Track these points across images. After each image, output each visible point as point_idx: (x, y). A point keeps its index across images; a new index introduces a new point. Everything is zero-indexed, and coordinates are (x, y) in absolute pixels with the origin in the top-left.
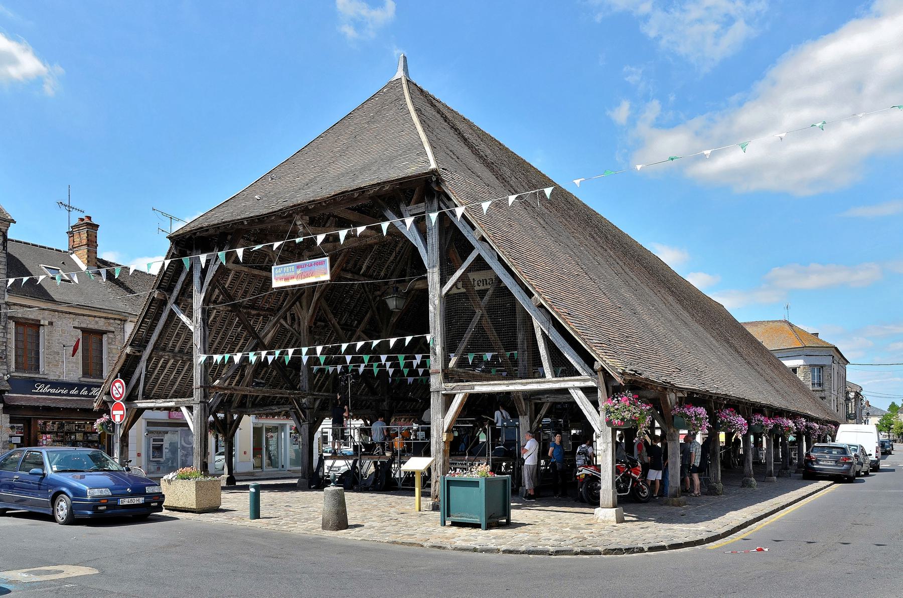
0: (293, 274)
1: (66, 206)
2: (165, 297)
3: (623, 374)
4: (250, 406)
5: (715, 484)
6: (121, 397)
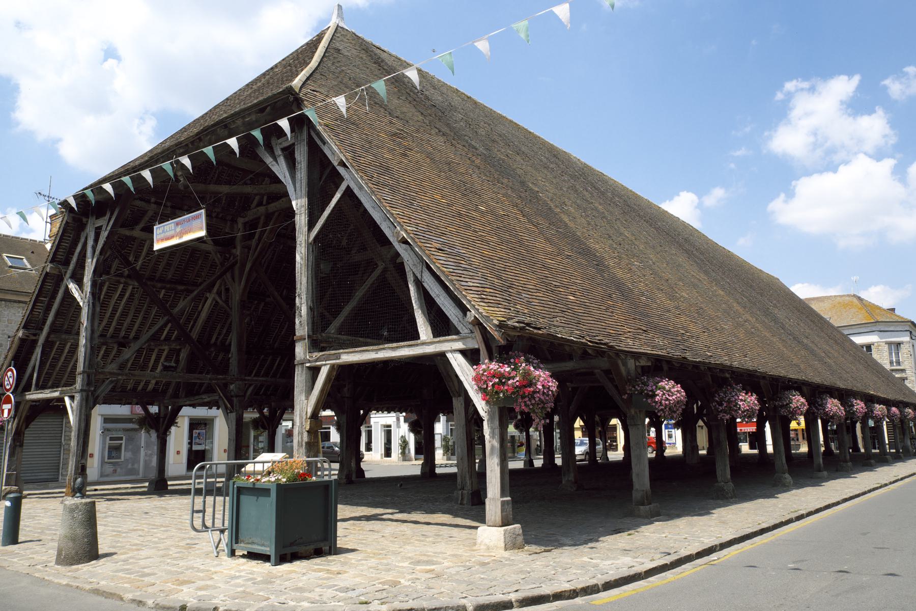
0: (172, 233)
1: (44, 196)
2: (60, 272)
3: (501, 326)
4: (183, 396)
5: (723, 483)
6: (10, 388)
